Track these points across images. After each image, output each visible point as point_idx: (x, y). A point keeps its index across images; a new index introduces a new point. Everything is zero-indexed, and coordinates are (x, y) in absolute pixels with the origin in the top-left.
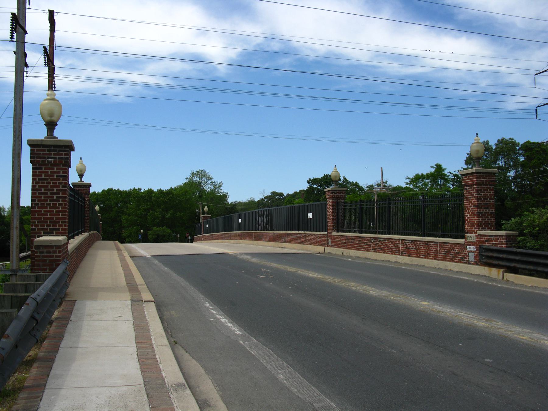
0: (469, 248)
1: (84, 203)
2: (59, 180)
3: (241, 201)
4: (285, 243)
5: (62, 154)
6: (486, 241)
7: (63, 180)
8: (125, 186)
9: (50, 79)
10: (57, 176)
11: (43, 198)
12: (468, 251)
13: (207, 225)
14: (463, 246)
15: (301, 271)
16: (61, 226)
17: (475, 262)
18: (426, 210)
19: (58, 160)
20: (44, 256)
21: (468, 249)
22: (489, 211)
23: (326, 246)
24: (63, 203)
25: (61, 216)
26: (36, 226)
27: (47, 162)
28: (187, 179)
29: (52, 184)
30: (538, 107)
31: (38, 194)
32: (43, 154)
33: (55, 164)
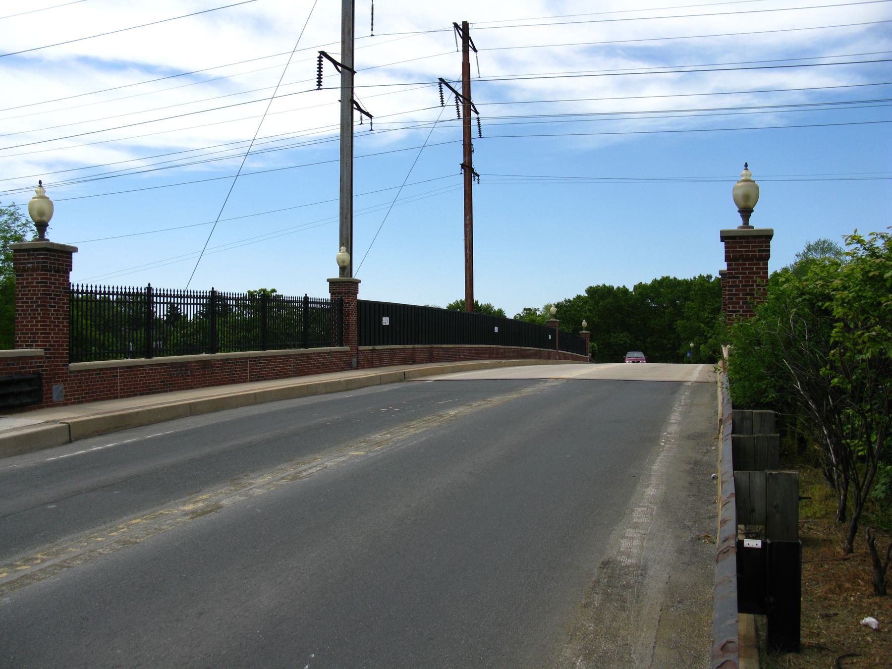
5: (39, 259)
9: (465, 127)
13: (550, 336)
15: (480, 405)
18: (144, 316)
27: (26, 268)
28: (797, 255)
32: (24, 259)
33: (34, 270)
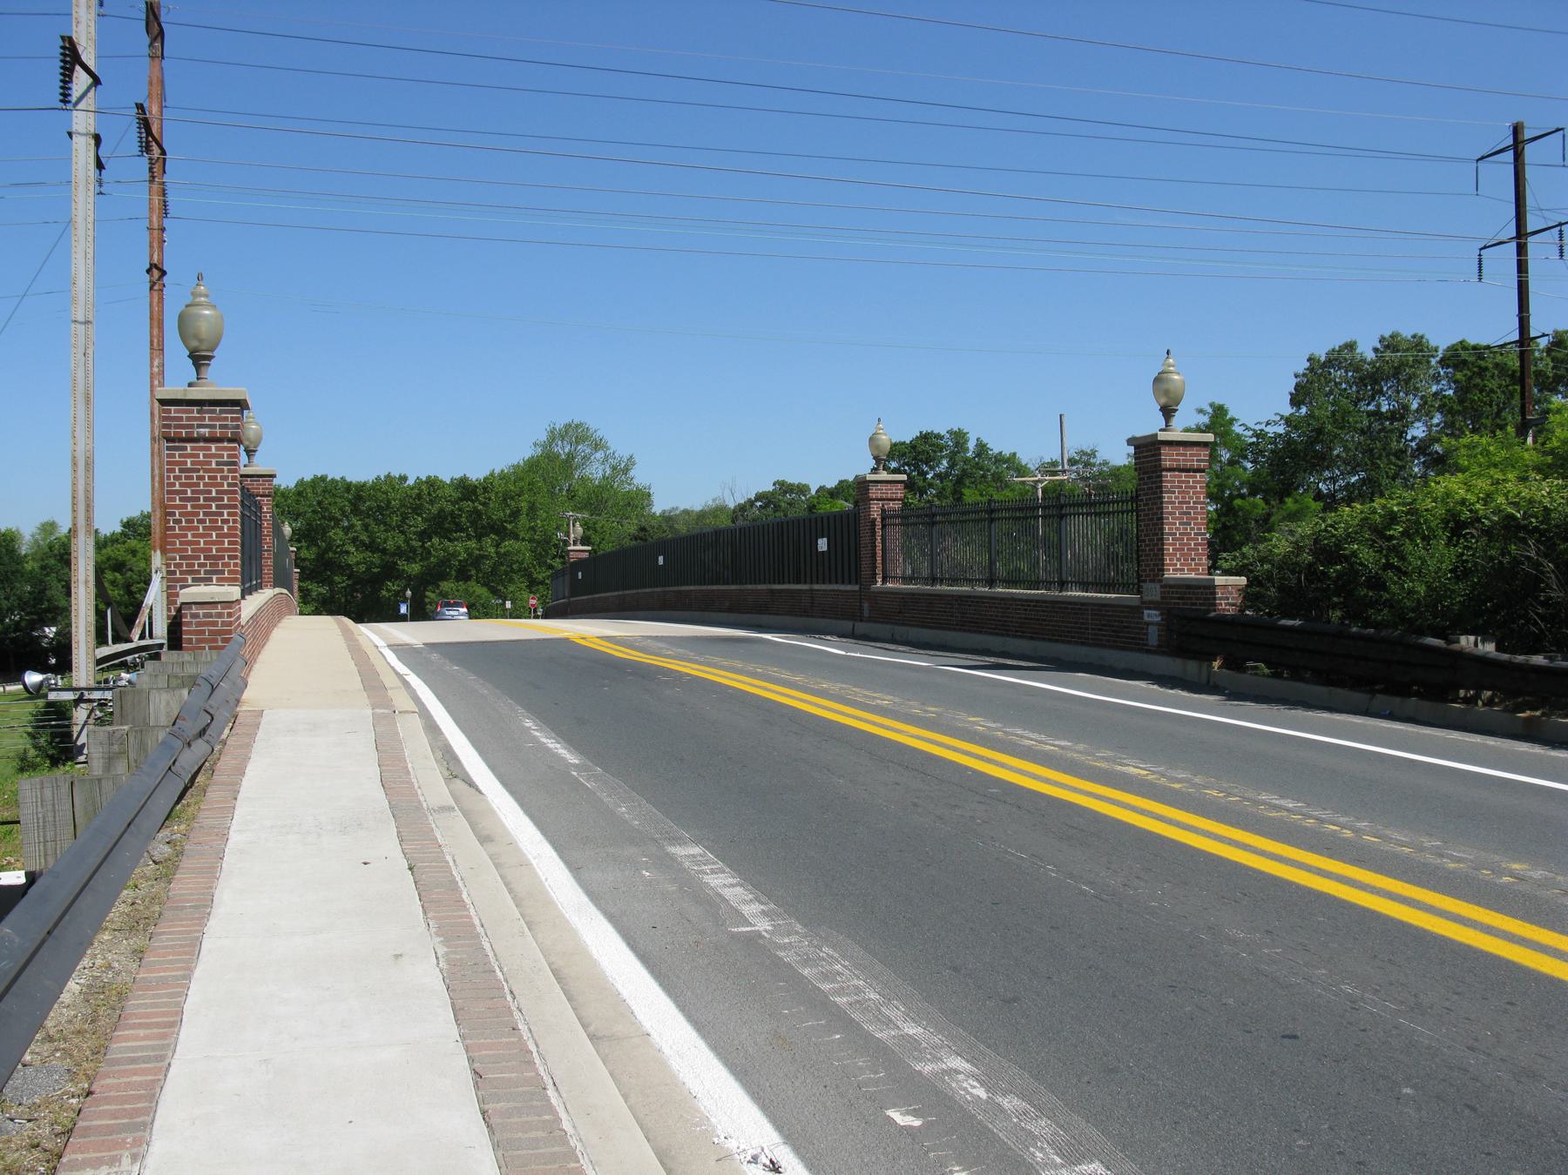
0: (1149, 615)
1: (261, 517)
2: (222, 471)
3: (689, 508)
4: (766, 614)
6: (1179, 598)
7: (229, 471)
8: (360, 469)
10: (218, 463)
11: (189, 509)
12: (1145, 623)
13: (580, 574)
14: (1136, 610)
16: (227, 565)
17: (1159, 646)
19: (218, 430)
20: (199, 624)
21: (1146, 618)
22: (1192, 529)
23: (855, 620)
24: (231, 518)
25: (226, 545)
26: (176, 565)
29: (207, 480)
30: (1485, 247)
31: (180, 501)
